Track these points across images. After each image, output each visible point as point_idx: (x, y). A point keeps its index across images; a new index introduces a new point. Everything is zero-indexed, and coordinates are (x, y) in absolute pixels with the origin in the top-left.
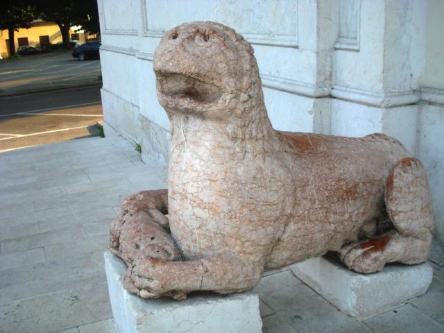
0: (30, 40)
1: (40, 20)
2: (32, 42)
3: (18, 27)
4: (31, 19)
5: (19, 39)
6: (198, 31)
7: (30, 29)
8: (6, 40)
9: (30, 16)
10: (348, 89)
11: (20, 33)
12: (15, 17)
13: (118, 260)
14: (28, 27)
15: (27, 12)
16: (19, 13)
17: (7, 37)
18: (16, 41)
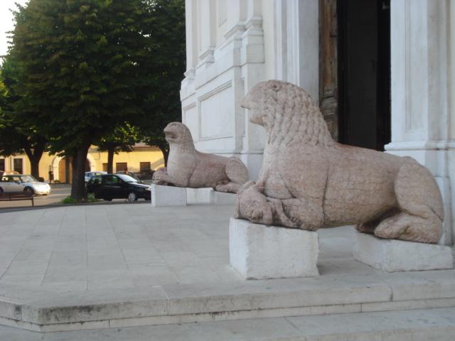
0: (129, 166)
1: (142, 144)
2: (131, 168)
3: (119, 150)
4: (132, 142)
5: (117, 163)
6: (59, 9)
7: (130, 153)
8: (104, 164)
9: (132, 138)
10: (357, 308)
11: (119, 157)
12: (116, 138)
13: (84, 304)
14: (128, 150)
15: (130, 134)
16: (122, 135)
17: (106, 161)
18: (114, 166)
